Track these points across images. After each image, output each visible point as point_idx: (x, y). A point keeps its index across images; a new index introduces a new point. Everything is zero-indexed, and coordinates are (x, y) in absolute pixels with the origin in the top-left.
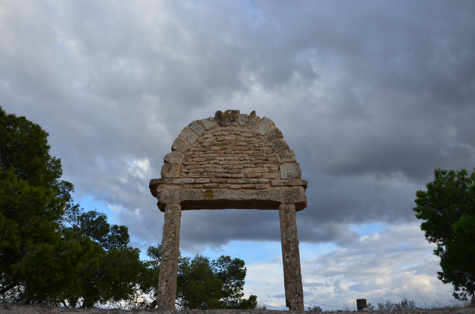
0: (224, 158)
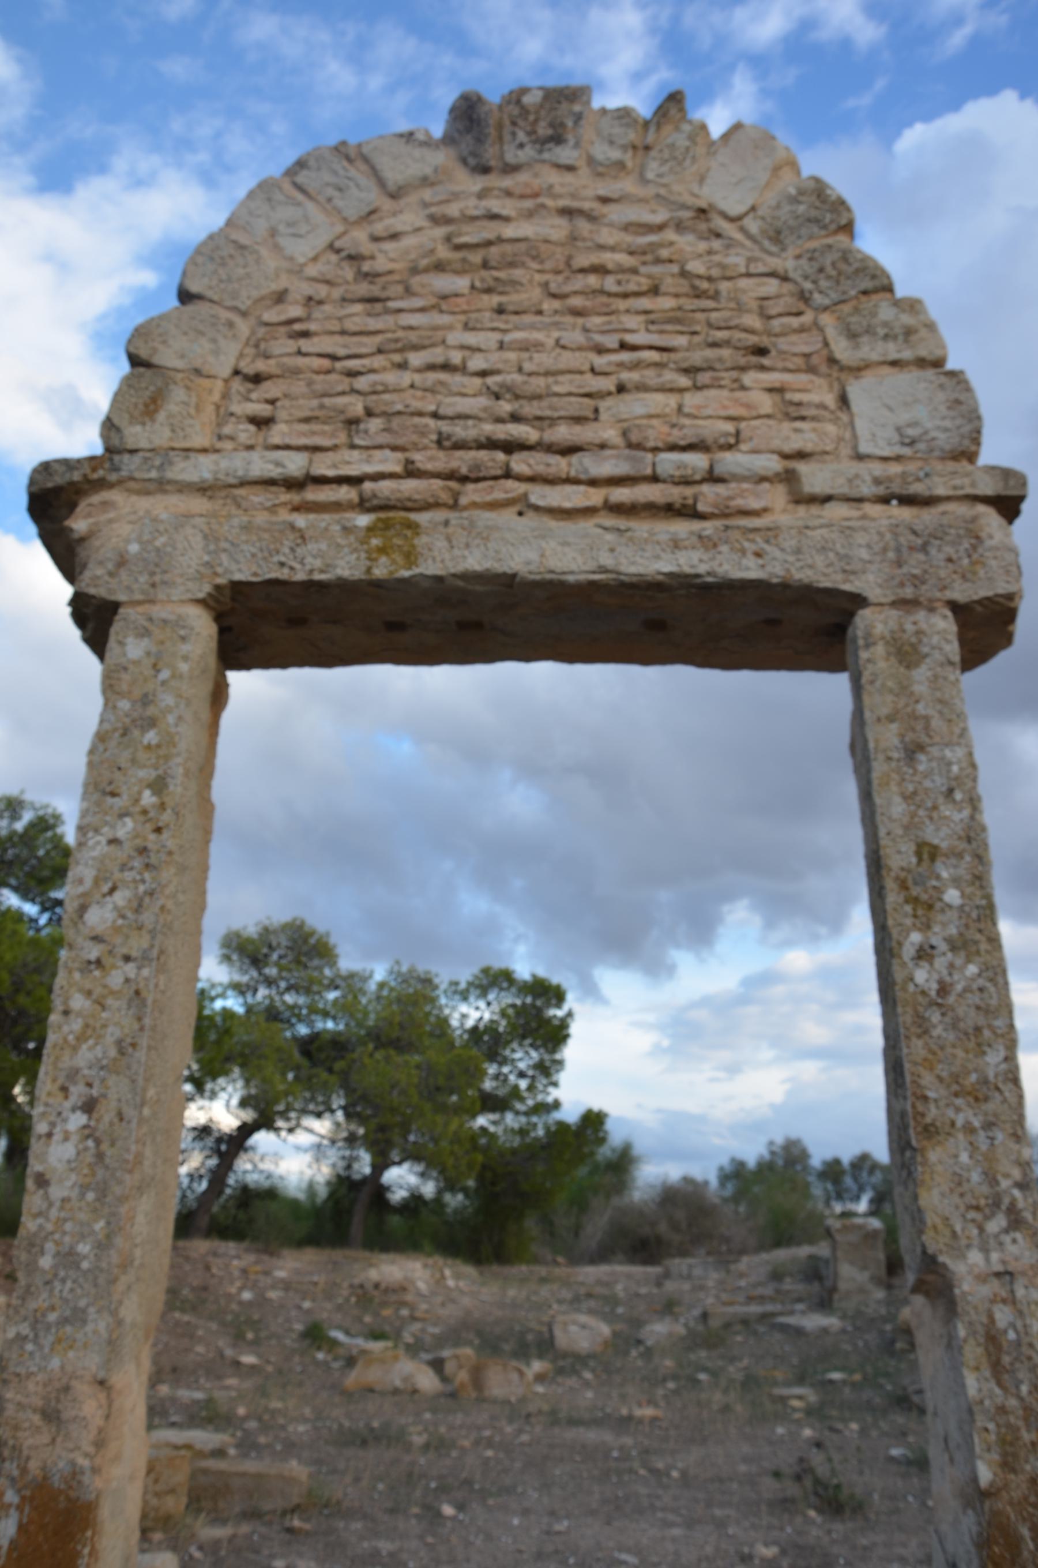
0: (496, 336)
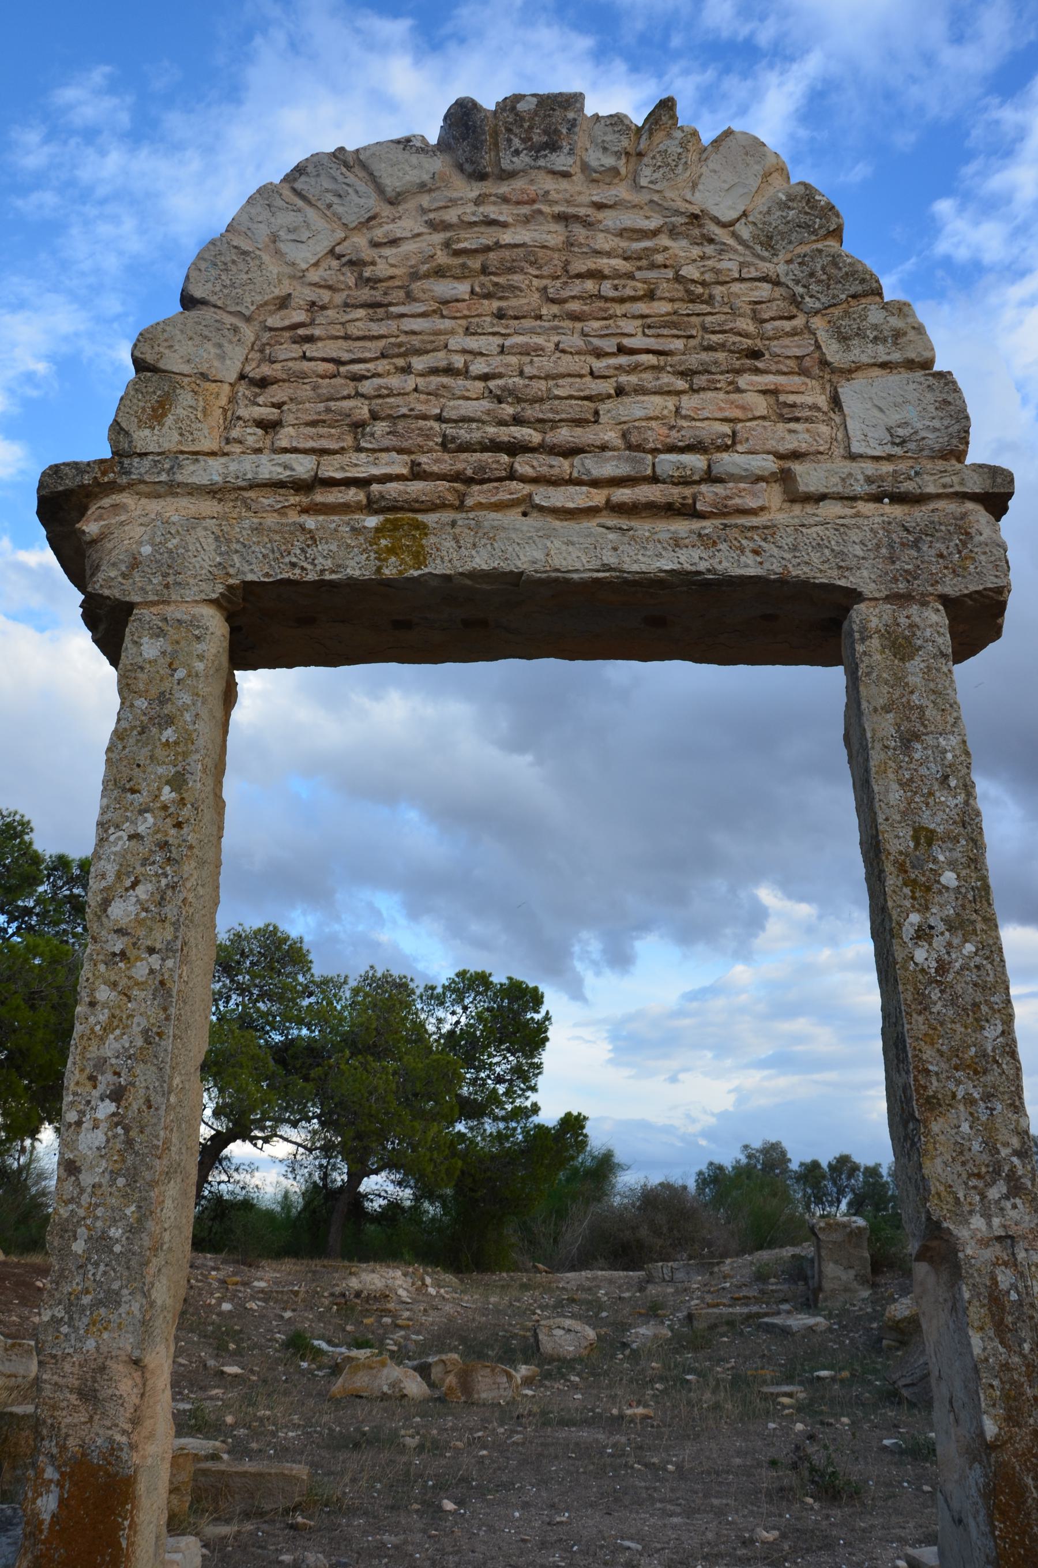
0: (498, 340)
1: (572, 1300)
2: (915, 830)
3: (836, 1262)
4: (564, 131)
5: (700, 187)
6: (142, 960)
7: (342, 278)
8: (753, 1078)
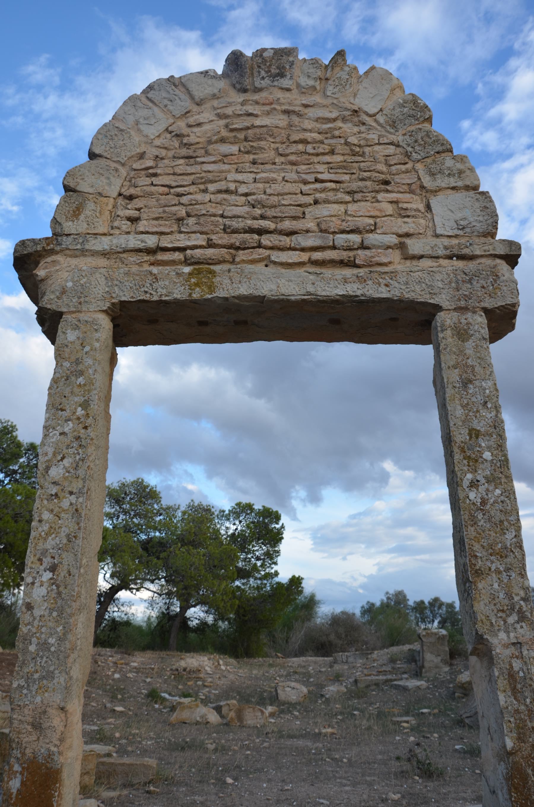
0: (253, 176)
1: (295, 672)
2: (470, 430)
3: (431, 653)
4: (288, 67)
5: (358, 96)
6: (66, 498)
7: (172, 143)
8: (385, 558)
